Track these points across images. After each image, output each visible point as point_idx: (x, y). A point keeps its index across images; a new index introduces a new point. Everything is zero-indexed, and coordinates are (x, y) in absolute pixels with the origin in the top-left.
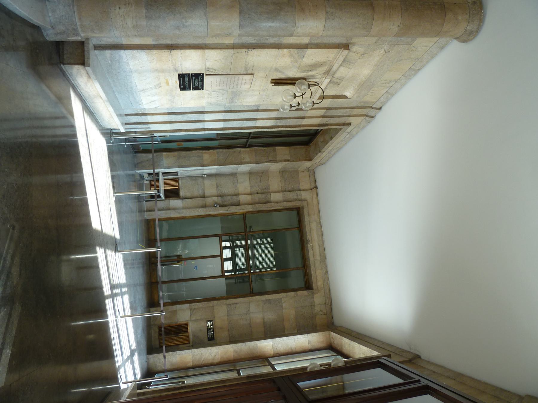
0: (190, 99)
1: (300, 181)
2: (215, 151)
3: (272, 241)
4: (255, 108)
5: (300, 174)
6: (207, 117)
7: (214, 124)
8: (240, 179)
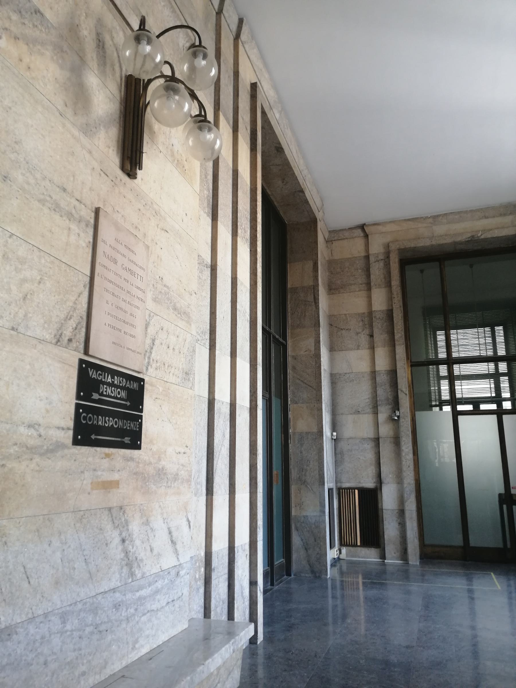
0: (169, 423)
1: (350, 256)
2: (291, 406)
3: (443, 332)
4: (208, 273)
5: (336, 257)
6: (223, 396)
7: (240, 380)
8: (342, 368)
